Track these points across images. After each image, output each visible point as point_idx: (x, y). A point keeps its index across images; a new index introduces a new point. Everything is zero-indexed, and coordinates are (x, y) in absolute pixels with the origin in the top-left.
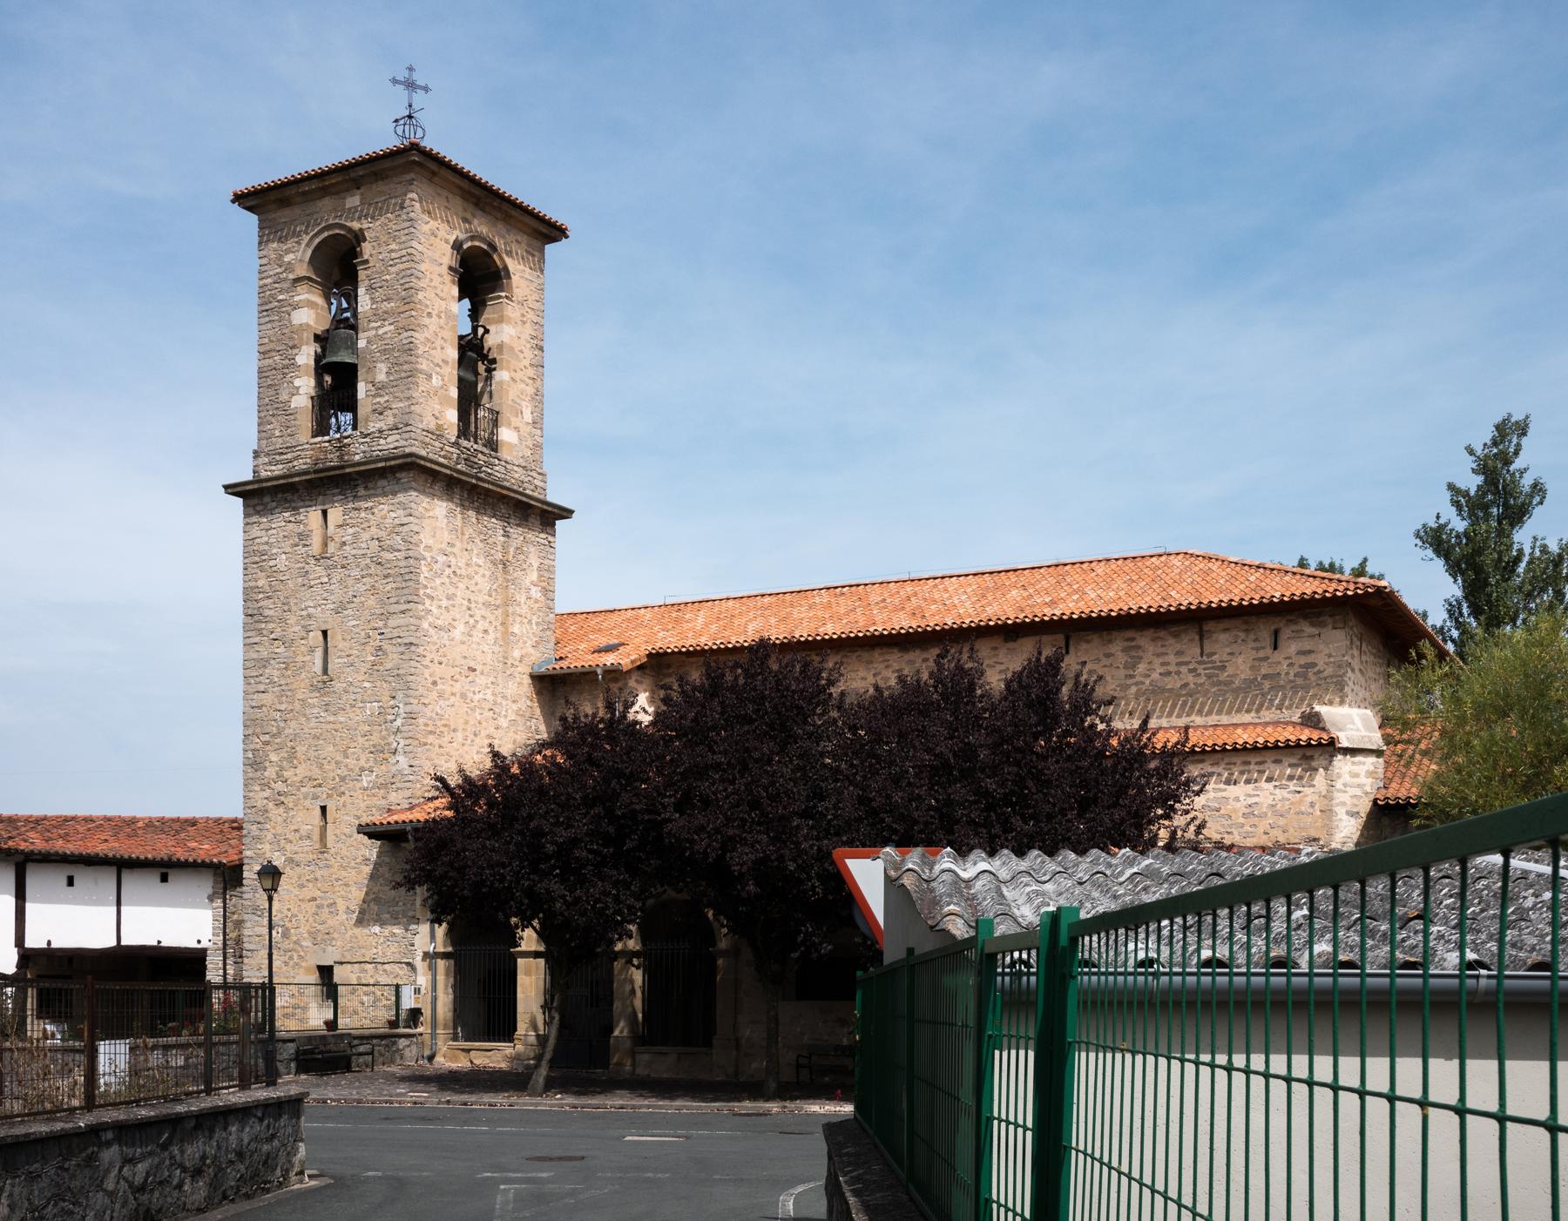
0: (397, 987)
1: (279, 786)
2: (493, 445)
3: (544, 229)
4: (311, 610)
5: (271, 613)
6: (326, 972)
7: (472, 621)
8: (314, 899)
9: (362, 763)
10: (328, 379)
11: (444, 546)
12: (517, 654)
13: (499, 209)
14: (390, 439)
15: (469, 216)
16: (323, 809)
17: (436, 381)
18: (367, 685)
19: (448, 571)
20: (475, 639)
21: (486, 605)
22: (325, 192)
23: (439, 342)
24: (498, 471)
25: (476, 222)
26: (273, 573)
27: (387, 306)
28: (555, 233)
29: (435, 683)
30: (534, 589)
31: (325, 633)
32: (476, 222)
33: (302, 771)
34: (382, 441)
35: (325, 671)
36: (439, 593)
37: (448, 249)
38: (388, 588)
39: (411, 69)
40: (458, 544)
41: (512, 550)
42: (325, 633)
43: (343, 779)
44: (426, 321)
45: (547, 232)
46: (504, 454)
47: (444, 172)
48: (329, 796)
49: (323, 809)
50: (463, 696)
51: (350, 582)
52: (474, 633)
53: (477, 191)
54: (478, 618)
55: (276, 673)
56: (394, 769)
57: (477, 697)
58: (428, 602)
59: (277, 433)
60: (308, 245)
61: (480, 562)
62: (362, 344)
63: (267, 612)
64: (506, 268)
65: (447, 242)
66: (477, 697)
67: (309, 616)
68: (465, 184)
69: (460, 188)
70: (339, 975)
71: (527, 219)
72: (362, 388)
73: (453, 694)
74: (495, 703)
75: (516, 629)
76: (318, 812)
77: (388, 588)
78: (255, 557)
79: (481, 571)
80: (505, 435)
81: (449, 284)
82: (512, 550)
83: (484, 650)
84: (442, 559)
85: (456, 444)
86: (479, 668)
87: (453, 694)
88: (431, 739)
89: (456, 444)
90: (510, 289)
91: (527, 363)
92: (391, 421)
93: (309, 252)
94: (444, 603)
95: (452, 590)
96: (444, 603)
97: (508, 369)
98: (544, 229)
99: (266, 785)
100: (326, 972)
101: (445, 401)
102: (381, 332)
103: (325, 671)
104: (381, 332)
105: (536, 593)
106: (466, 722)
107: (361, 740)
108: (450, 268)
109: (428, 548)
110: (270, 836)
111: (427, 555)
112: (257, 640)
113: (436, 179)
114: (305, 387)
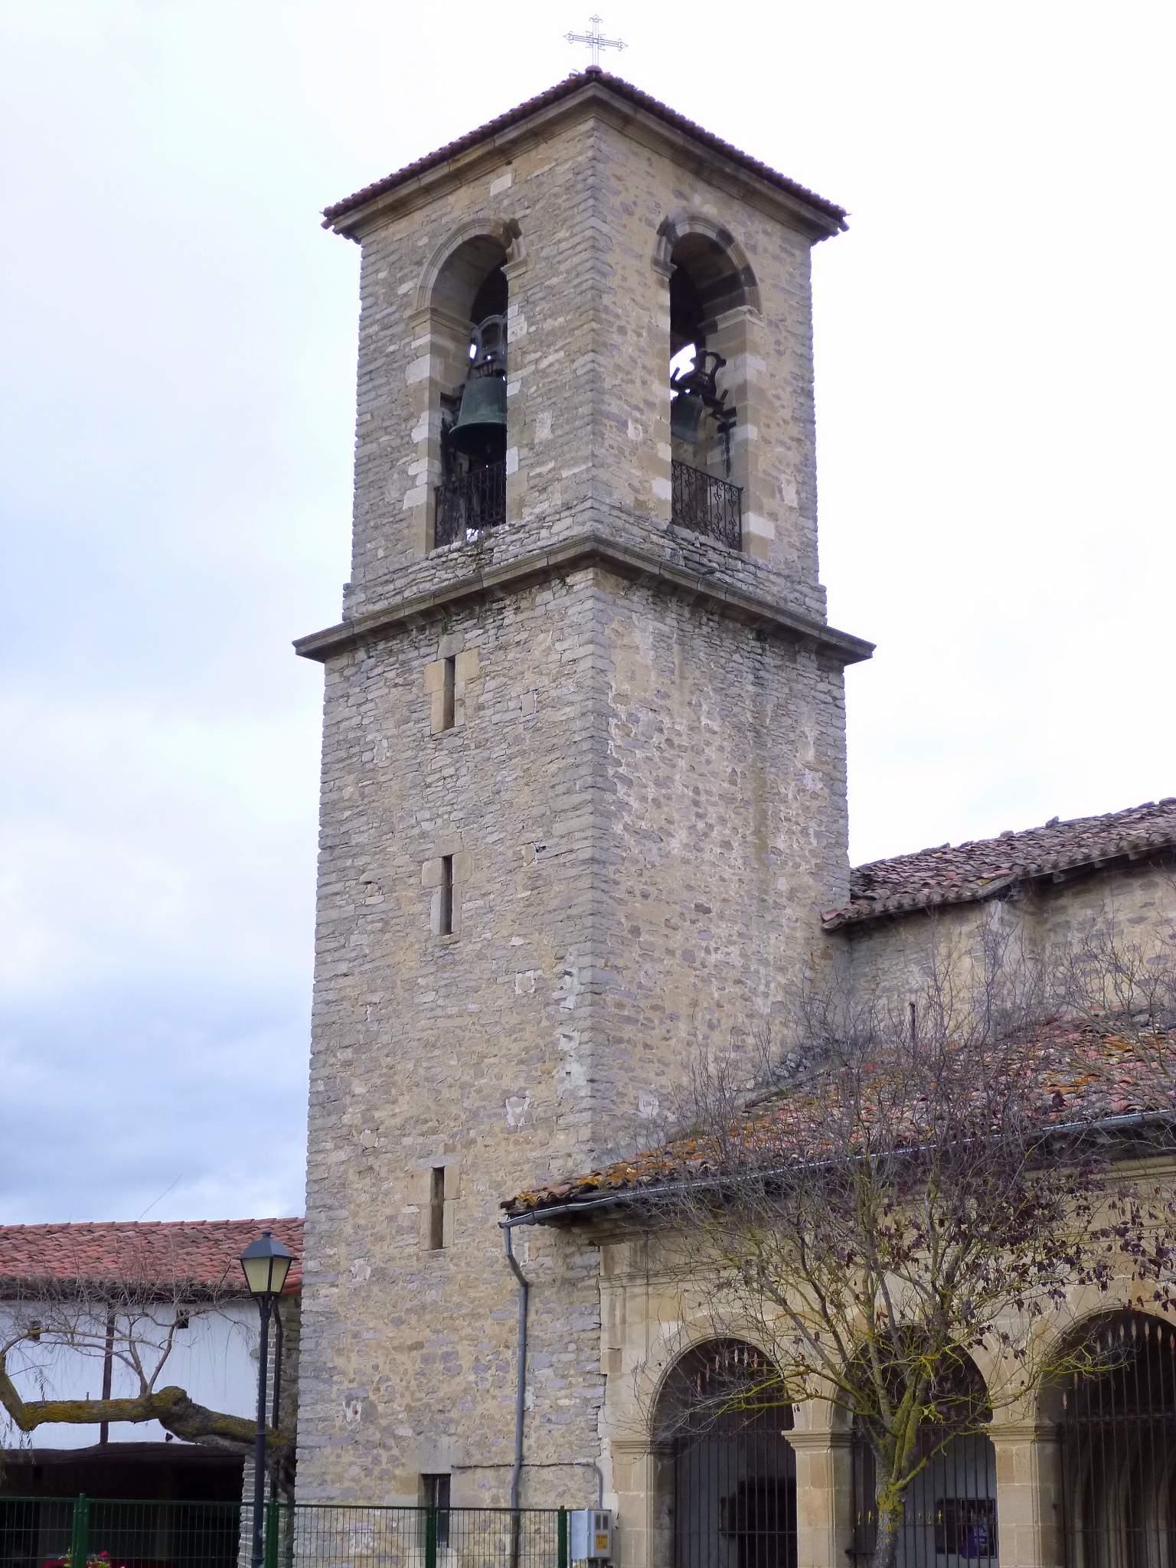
0: (563, 1513)
1: (366, 1138)
2: (736, 541)
3: (807, 213)
4: (426, 826)
5: (362, 839)
6: (436, 1485)
7: (701, 825)
8: (418, 1346)
9: (506, 1083)
10: (464, 461)
11: (649, 695)
12: (782, 884)
13: (734, 180)
14: (556, 529)
15: (686, 190)
16: (439, 1173)
17: (633, 432)
18: (517, 941)
19: (656, 739)
20: (707, 856)
21: (728, 799)
22: (458, 178)
23: (638, 374)
24: (742, 580)
25: (697, 199)
26: (367, 771)
27: (550, 324)
28: (825, 221)
29: (636, 931)
30: (809, 776)
31: (448, 860)
32: (697, 199)
33: (405, 1106)
34: (544, 533)
35: (447, 928)
36: (644, 775)
37: (652, 236)
38: (553, 768)
39: (596, 20)
40: (675, 694)
41: (769, 708)
42: (448, 860)
43: (474, 1115)
44: (616, 338)
45: (817, 219)
46: (753, 553)
47: (642, 117)
48: (449, 1149)
49: (439, 1173)
50: (688, 956)
51: (489, 767)
52: (706, 846)
53: (698, 150)
54: (712, 819)
55: (364, 940)
56: (561, 1089)
57: (714, 958)
58: (621, 789)
59: (381, 553)
60: (432, 264)
61: (715, 726)
62: (512, 390)
63: (356, 839)
64: (748, 269)
65: (650, 224)
66: (714, 958)
67: (423, 835)
68: (678, 139)
69: (670, 144)
70: (460, 1491)
71: (780, 197)
72: (512, 456)
73: (670, 952)
74: (746, 969)
75: (781, 842)
76: (428, 1180)
77: (553, 768)
78: (341, 752)
79: (717, 741)
80: (755, 524)
81: (654, 287)
82: (769, 708)
83: (727, 871)
84: (645, 716)
85: (668, 533)
86: (715, 907)
87: (670, 952)
88: (628, 1031)
89: (668, 533)
90: (756, 303)
91: (787, 414)
92: (558, 500)
93: (435, 272)
94: (651, 792)
95: (663, 771)
96: (651, 792)
97: (756, 423)
98: (807, 213)
99: (345, 1138)
100: (436, 1485)
101: (651, 463)
102: (544, 364)
103: (447, 928)
104: (544, 364)
105: (812, 782)
106: (695, 1004)
107: (505, 1041)
108: (656, 262)
109: (622, 697)
110: (349, 1230)
111: (621, 709)
112: (338, 887)
113: (630, 130)
114: (422, 472)
